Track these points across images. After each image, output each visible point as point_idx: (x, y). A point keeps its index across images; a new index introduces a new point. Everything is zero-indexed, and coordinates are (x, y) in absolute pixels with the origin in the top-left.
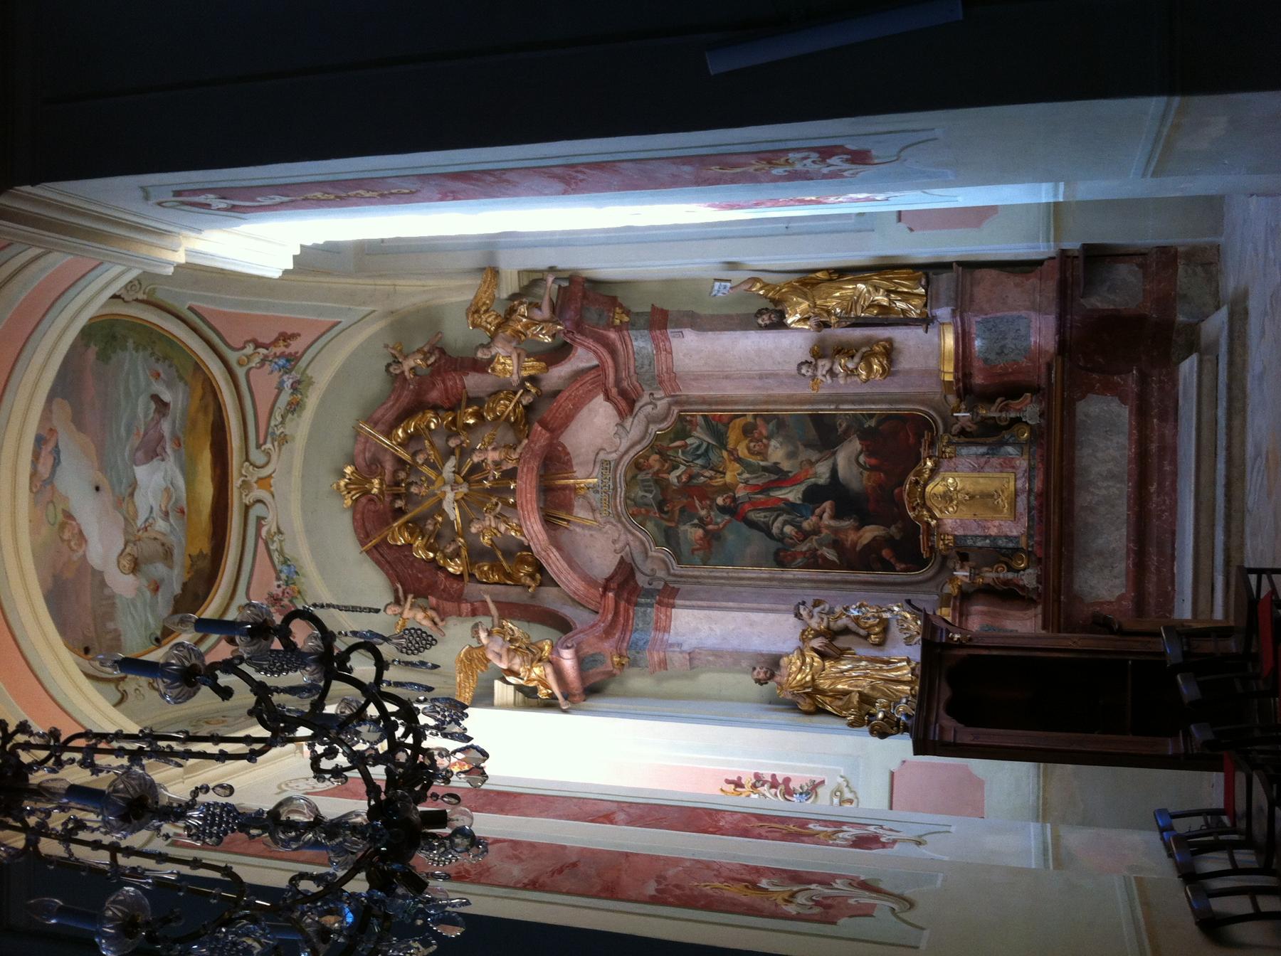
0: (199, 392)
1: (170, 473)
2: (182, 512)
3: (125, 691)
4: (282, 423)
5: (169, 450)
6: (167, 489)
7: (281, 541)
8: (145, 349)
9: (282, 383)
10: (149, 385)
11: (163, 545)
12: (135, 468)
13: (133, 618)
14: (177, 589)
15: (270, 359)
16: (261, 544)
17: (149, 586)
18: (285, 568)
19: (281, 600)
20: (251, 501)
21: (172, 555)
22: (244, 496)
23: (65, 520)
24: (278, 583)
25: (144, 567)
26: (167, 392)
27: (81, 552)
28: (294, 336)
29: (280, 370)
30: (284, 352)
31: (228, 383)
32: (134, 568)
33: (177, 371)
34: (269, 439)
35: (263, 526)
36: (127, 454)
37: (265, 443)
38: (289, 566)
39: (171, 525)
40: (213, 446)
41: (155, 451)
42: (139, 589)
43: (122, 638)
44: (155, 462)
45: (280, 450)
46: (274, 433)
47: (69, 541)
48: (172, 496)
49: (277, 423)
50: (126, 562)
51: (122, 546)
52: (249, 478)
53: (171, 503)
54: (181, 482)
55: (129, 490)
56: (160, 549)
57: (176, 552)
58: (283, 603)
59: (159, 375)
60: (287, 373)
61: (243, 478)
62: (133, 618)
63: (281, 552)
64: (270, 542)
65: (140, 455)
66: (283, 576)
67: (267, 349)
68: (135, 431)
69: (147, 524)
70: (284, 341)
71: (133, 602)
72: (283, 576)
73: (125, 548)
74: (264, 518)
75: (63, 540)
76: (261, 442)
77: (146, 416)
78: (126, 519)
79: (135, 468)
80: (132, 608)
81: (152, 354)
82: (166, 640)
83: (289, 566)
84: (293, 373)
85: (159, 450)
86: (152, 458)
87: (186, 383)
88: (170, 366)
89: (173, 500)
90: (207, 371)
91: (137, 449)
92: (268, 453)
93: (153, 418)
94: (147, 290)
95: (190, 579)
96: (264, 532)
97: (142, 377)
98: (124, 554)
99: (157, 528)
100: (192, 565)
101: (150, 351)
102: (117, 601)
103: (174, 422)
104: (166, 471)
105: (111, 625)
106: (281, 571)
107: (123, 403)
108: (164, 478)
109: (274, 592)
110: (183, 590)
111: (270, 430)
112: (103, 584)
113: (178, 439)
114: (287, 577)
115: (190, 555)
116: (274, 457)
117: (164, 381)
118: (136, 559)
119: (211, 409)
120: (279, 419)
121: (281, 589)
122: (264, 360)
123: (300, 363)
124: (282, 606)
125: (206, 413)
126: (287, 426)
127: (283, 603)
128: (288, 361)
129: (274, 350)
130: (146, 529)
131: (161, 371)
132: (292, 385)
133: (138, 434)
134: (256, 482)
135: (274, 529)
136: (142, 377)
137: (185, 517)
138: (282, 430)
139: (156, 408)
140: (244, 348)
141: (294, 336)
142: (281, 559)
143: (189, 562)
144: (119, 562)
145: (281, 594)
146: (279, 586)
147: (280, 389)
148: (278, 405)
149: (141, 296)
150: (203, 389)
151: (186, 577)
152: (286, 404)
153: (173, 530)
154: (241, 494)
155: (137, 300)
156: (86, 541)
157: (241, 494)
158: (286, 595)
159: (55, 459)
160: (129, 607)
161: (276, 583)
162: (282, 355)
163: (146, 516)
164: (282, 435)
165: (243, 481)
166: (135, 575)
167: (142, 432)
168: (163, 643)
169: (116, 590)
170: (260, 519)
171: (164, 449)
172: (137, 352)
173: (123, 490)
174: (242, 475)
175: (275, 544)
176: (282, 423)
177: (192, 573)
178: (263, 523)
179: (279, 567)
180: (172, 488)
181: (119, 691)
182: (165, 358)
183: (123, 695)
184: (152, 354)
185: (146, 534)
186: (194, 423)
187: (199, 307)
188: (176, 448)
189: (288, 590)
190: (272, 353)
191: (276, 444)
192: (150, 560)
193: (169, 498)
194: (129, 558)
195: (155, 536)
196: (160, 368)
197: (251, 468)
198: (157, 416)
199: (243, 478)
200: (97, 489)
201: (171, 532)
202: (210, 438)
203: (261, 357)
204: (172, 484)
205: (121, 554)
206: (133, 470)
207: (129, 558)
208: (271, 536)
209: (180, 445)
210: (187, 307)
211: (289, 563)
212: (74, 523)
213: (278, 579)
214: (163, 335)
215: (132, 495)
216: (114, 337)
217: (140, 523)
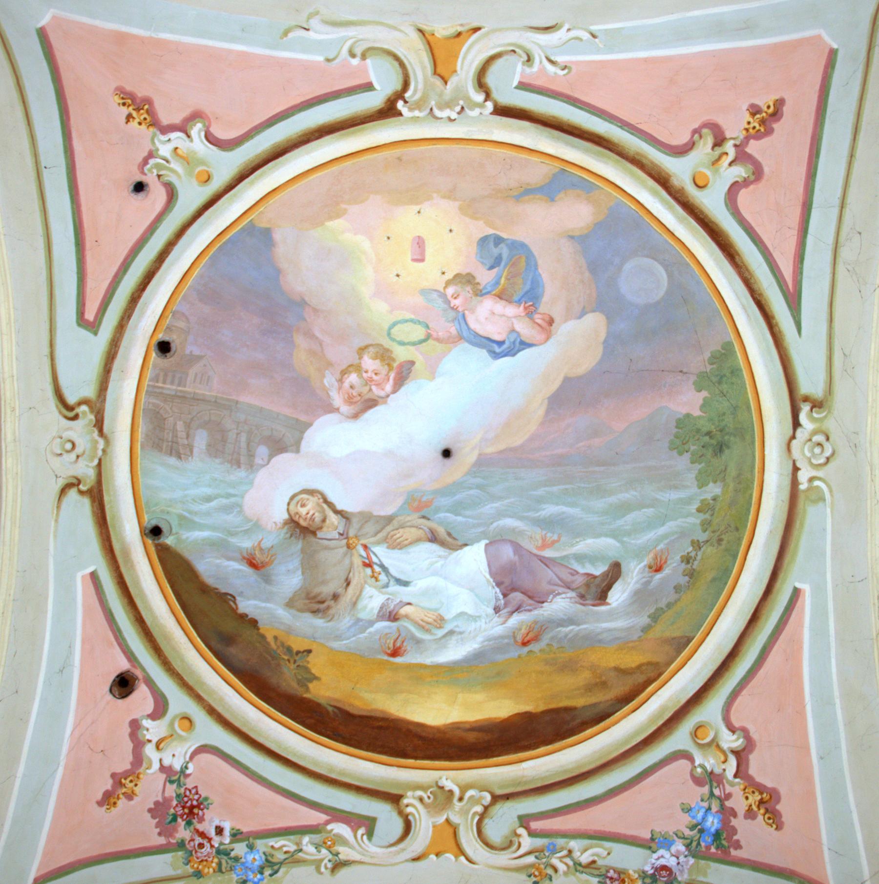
0: (631, 660)
1: (473, 626)
2: (395, 653)
3: (76, 417)
4: (579, 867)
5: (515, 620)
6: (440, 621)
7: (317, 864)
8: (705, 525)
9: (666, 843)
10: (638, 554)
11: (335, 597)
12: (483, 543)
13: (208, 499)
14: (245, 606)
15: (717, 792)
16: (317, 817)
17: (261, 549)
18: (255, 858)
19: (189, 823)
20: (409, 810)
21: (315, 612)
22: (420, 793)
23: (395, 365)
24: (227, 832)
25: (298, 546)
26: (626, 595)
27: (337, 400)
28: (775, 819)
29: (692, 828)
30: (735, 815)
31: (652, 720)
32: (297, 524)
33: (669, 606)
34: (539, 842)
35: (355, 831)
36: (509, 522)
37: (532, 834)
38: (261, 871)
39: (371, 623)
40: (528, 718)
41: (514, 589)
42: (256, 526)
43: (172, 461)
44: (493, 592)
45: (518, 869)
46: (554, 850)
47: (358, 368)
48: (428, 631)
49: (576, 854)
50: (309, 509)
51: (339, 507)
52: (457, 805)
53: (413, 629)
54: (454, 653)
55: (441, 531)
56: (327, 590)
57: (319, 622)
58: (181, 823)
59: (659, 570)
60: (688, 846)
61: (457, 791)
62: (208, 499)
63: (294, 859)
64: (317, 838)
65: (507, 553)
66: (240, 849)
67: (735, 776)
68: (551, 536)
69: (377, 569)
70: (761, 802)
71: (236, 507)
72: (240, 849)
73: (337, 512)
74: (370, 834)
75: (362, 350)
76: (534, 825)
77: (580, 558)
78: (389, 519)
79: (483, 543)
80: (224, 501)
81: (697, 545)
82: (152, 550)
83: (261, 871)
84: (692, 861)
85: (517, 596)
86: (499, 584)
87: (646, 629)
88: (677, 589)
89: (419, 634)
90: (673, 666)
91: (517, 548)
92: (511, 843)
93: (575, 573)
94: (817, 483)
95: (263, 637)
96: (340, 829)
97: (651, 535)
98: (325, 506)
99: (369, 590)
100: (289, 650)
101: (702, 537)
102: (241, 473)
103: (570, 621)
104: (475, 618)
105: (201, 440)
106: (251, 847)
107: (599, 504)
108: (462, 614)
109: (208, 814)
110: (243, 617)
111: (560, 842)
112: (278, 447)
113: (536, 639)
114: (237, 859)
115: (309, 651)
116: (504, 859)
117: (648, 583)
118: (314, 533)
119: (601, 697)
120: (585, 858)
121: (212, 833)
122: (713, 778)
123: (714, 865)
124: (174, 819)
125: (589, 688)
126: (572, 878)
127: (181, 823)
128: (717, 835)
129: (736, 788)
130: (368, 565)
131: (667, 571)
132: (664, 868)
133: (544, 546)
134: (448, 821)
135: (345, 853)
136: (651, 535)
137: (386, 658)
138: (562, 867)
139: (595, 577)
140: (732, 729)
141: (775, 819)
142: (280, 856)
143: (297, 645)
144: (311, 492)
145: (200, 827)
146: (219, 831)
147: (650, 844)
148: (618, 848)
149: (803, 476)
150: (639, 667)
151: (267, 629)
152: (619, 865)
153: (362, 625)
154: (424, 788)
155: (796, 469)
156: (356, 416)
157: (424, 788)
158: (198, 840)
159: (500, 343)
160: (228, 496)
161: (227, 826)
162: (727, 813)
163: (392, 571)
164: (550, 871)
165: (451, 792)
166: (286, 523)
167: (548, 553)
168: (149, 541)
169: (261, 476)
170: (369, 824)
171: (518, 609)
172: (699, 510)
173: (442, 515)
174: (464, 789)
175: (311, 849)
176: (579, 867)
177: (273, 645)
178: (361, 831)
179: (262, 845)
180: (440, 633)
181: (80, 404)
182: (691, 574)
183: (70, 408)
184: (697, 545)
185: (357, 562)
186: (569, 666)
187: (804, 601)
188: (519, 638)
189: (207, 849)
190: (728, 789)
191: (531, 859)
192: (309, 564)
193: (424, 627)
194: (318, 517)
195: (354, 583)
196: (673, 569)
197: (479, 809)
198: (579, 580)
199: (457, 791)
200: (447, 453)
201: (359, 620)
202: (542, 708)
203: (718, 771)
204: (451, 633)
205: (326, 501)
206: (477, 540)
207: (318, 517)
208: (331, 843)
209: (525, 644)
210: (798, 585)
211: (267, 872)
212: (389, 387)
213: (237, 835)
214: (735, 557)
215: (434, 538)
216: (720, 448)
217: (381, 553)
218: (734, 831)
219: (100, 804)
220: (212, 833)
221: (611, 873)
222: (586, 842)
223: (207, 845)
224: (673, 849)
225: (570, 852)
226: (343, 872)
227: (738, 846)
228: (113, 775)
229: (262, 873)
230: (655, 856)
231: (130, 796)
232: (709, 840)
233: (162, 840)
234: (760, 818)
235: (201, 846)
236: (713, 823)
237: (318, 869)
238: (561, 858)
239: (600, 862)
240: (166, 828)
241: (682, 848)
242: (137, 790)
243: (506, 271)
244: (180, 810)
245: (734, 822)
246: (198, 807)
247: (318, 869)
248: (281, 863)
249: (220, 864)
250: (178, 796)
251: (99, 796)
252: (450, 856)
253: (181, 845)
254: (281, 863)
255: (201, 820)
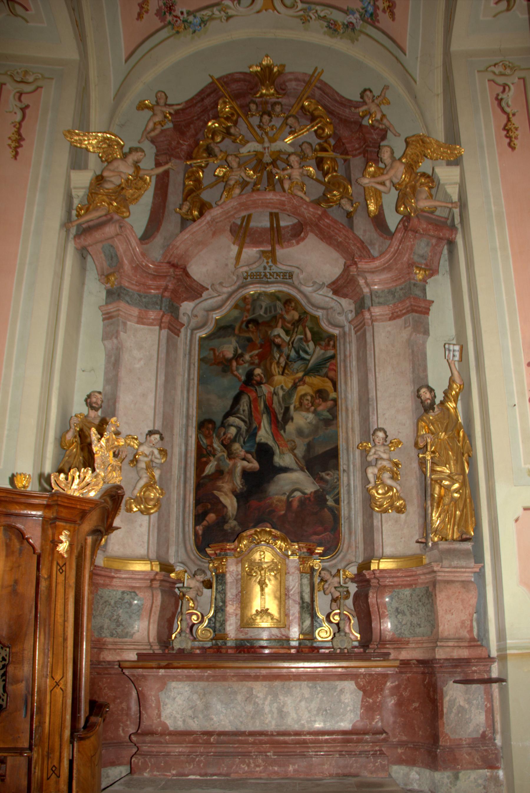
4: (320, 18)
7: (220, 18)
9: (353, 13)
18: (197, 21)
19: (170, 13)
29: (363, 9)
30: (378, 9)
46: (310, 10)
49: (319, 12)
58: (167, 14)
60: (361, 16)
63: (211, 18)
64: (219, 8)
66: (191, 18)
70: (389, 7)
72: (191, 18)
84: (361, 22)
106: (195, 17)
111: (313, 6)
114: (190, 23)
116: (291, 12)
120: (322, 14)
121: (180, 15)
124: (165, 14)
127: (167, 14)
128: (371, 15)
132: (351, 23)
135: (231, 12)
138: (313, 17)
142: (206, 18)
145: (175, 14)
146: (182, 13)
148: (335, 12)
158: (175, 19)
161: (184, 11)
162: (376, 7)
164: (309, 18)
175: (217, 13)
176: (320, 18)
179: (198, 15)
189: (179, 21)
211: (202, 25)
213: (189, 13)
218: (377, 15)
219: (137, 19)
220: (180, 15)
221: (332, 22)
222: (323, 8)
223: (179, 20)
224: (355, 16)
225: (317, 11)
226: (231, 21)
227: (378, 22)
228: (139, 5)
229: (200, 26)
230: (348, 17)
231: (147, 12)
232: (368, 15)
233: (162, 24)
234: (387, 14)
235: (177, 21)
236: (370, 9)
237: (221, 21)
238: (313, 14)
239: (328, 16)
240: (163, 19)
241: (358, 16)
242: (149, 8)
243: (47, 730)
244: (166, 10)
245: (378, 11)
246: (173, 6)
247: (221, 21)
248: (207, 21)
249: (185, 26)
250: (164, 4)
251: (136, 16)
252: (270, 11)
253: (170, 23)
254: (207, 21)
255: (174, 11)
